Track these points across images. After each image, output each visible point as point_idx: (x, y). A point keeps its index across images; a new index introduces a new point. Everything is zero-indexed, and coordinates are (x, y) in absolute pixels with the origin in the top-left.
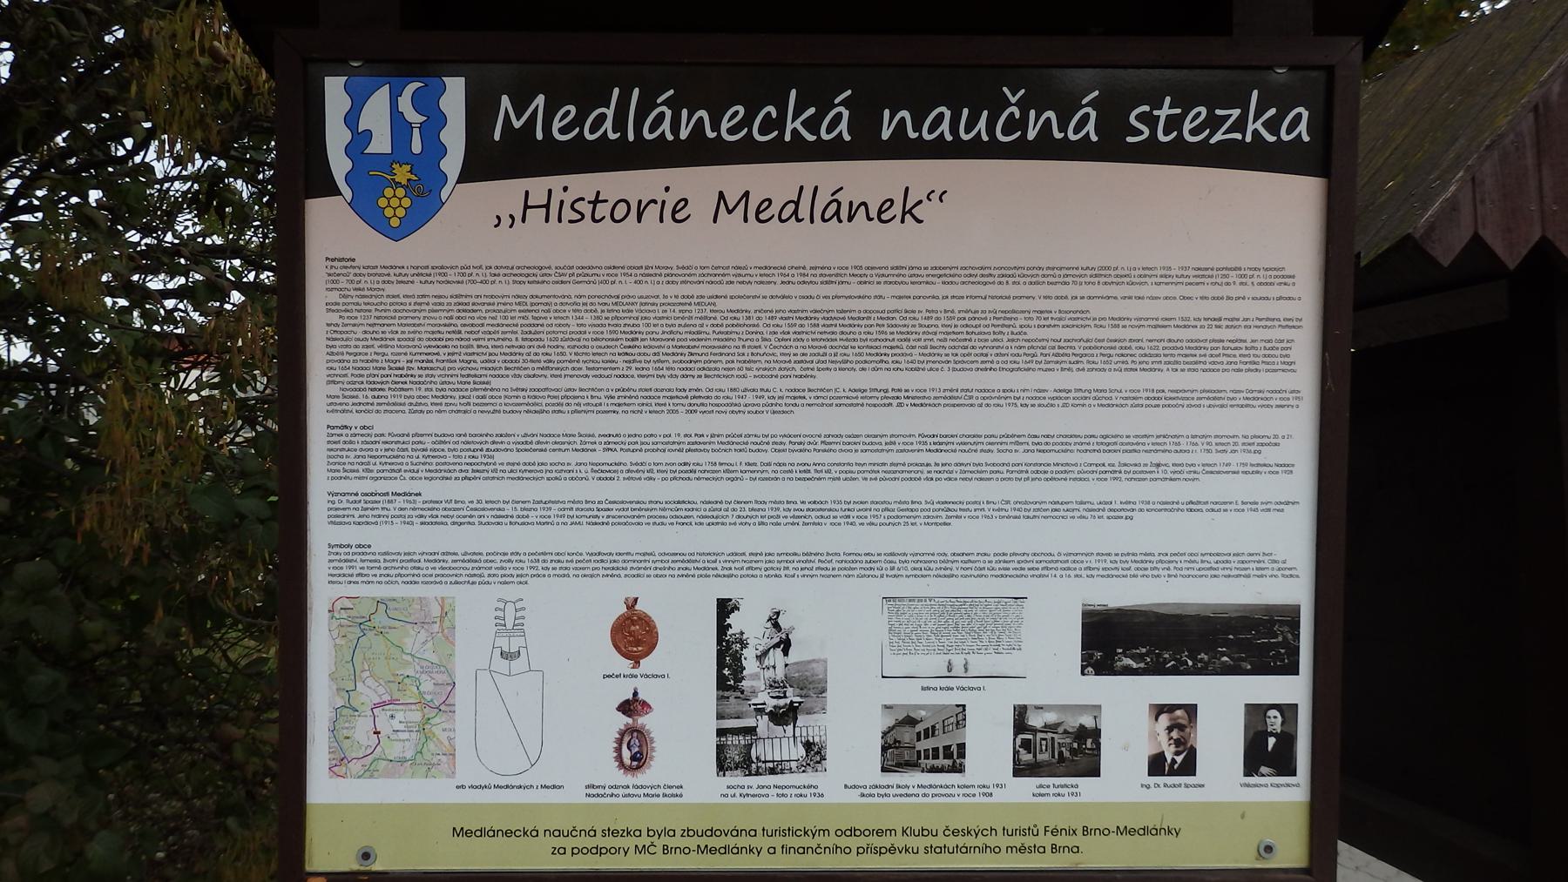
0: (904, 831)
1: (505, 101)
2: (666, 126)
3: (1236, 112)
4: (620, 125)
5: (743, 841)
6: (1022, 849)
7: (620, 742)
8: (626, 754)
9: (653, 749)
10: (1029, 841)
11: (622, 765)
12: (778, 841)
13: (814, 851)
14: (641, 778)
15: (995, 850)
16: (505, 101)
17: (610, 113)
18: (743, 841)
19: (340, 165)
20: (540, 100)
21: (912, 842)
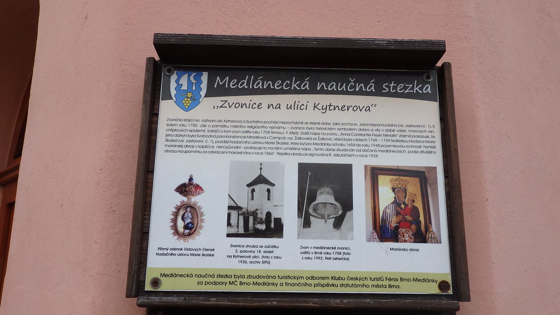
0: (332, 278)
1: (218, 78)
2: (260, 85)
3: (411, 86)
4: (248, 84)
5: (271, 281)
6: (377, 286)
7: (176, 214)
8: (180, 224)
9: (202, 221)
10: (380, 283)
11: (176, 232)
12: (284, 281)
13: (298, 285)
14: (194, 242)
15: (367, 286)
16: (218, 78)
17: (246, 81)
18: (271, 281)
19: (173, 92)
20: (227, 78)
21: (335, 282)
